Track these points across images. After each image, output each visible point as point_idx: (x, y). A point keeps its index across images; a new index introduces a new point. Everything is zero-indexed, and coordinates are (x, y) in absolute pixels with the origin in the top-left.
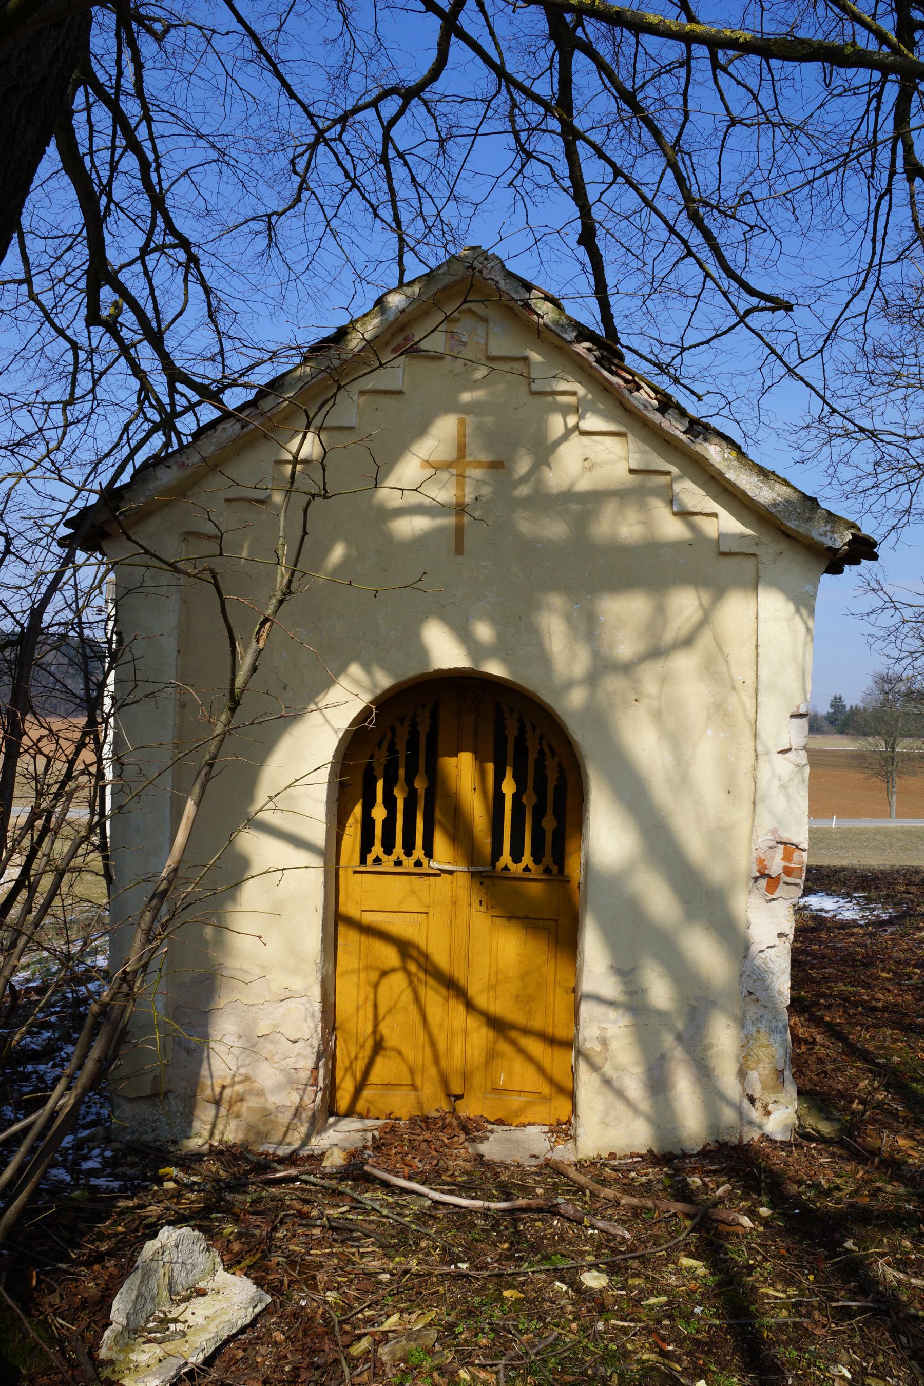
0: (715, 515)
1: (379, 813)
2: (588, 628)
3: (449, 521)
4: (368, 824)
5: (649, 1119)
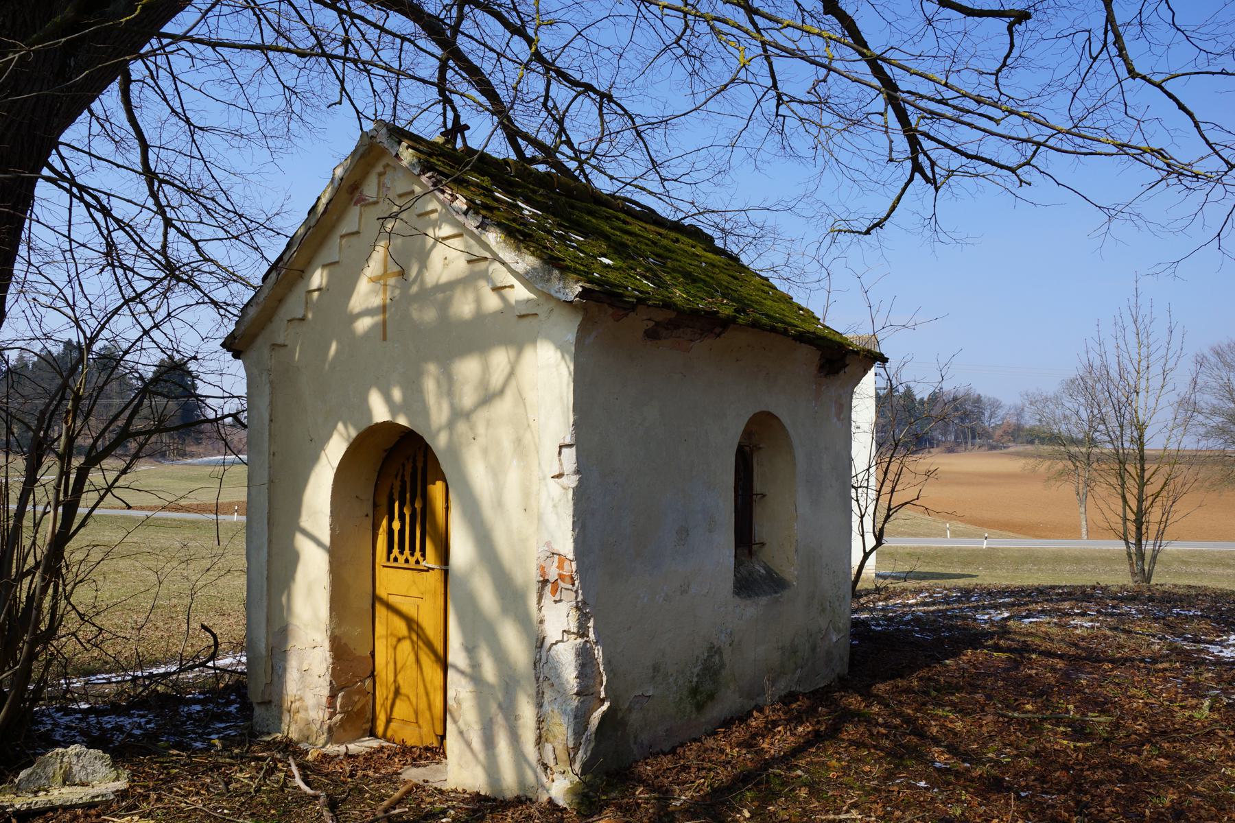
0: (512, 286)
1: (396, 525)
2: (449, 386)
3: (378, 318)
4: (390, 532)
5: (484, 767)
